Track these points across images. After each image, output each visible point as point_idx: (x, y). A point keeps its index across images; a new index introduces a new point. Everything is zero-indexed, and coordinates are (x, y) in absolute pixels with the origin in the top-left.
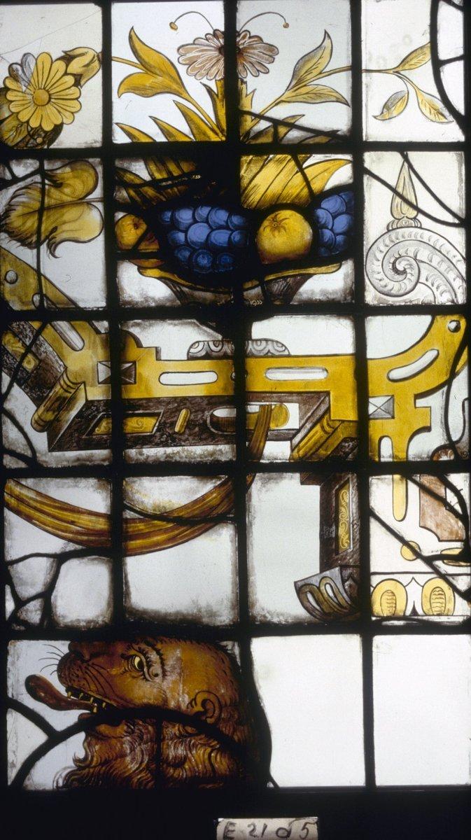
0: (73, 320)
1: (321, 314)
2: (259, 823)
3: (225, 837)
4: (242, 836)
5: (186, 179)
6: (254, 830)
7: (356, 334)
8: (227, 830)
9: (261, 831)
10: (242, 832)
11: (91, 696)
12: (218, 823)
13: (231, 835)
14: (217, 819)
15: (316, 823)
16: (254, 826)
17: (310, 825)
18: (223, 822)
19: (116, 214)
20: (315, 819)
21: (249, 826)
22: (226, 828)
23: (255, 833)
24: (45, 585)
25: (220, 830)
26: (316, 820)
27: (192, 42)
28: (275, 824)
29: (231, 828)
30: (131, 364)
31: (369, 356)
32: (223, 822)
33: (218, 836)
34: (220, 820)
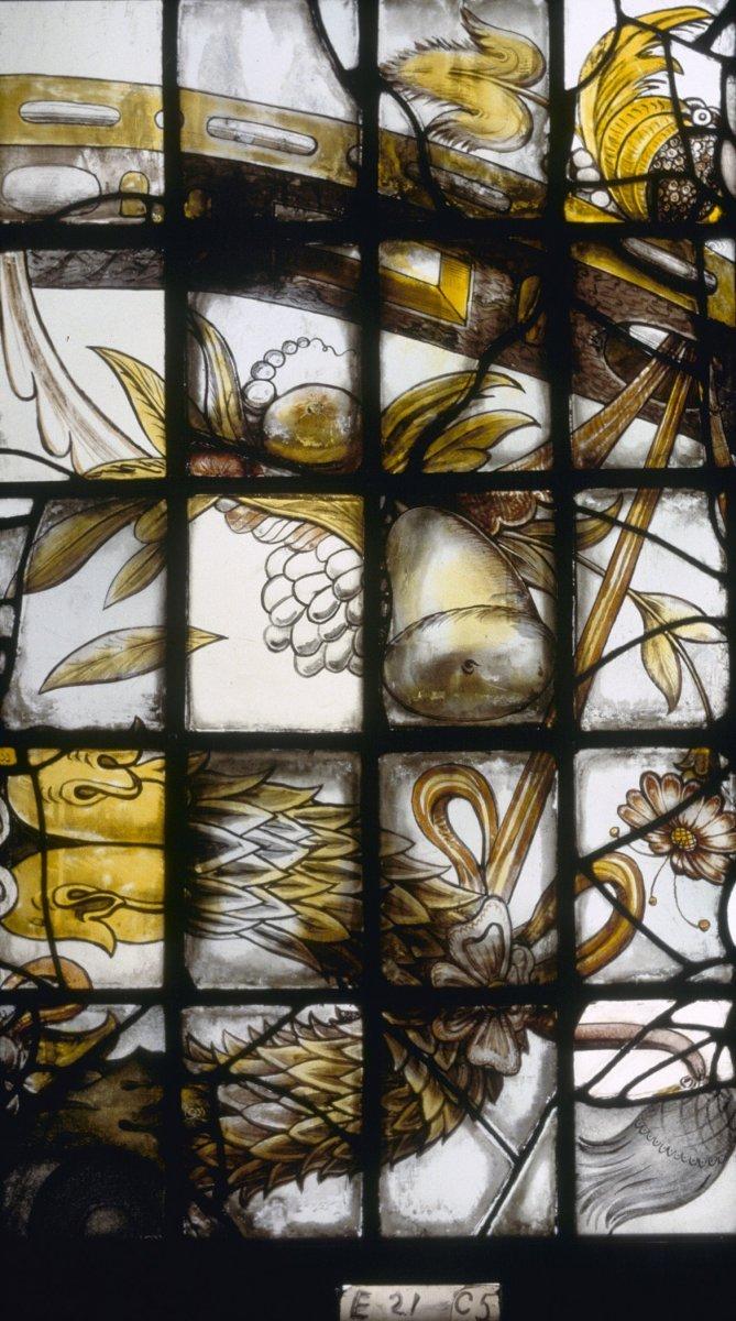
0: (41, 248)
1: (549, 406)
2: (408, 1292)
3: (354, 1315)
4: (380, 1312)
5: (279, 209)
6: (399, 1304)
7: (73, 1064)
8: (356, 1305)
9: (410, 1306)
10: (380, 1306)
11: (629, 383)
12: (341, 1293)
13: (362, 1311)
14: (340, 1286)
15: (498, 1293)
16: (400, 1298)
17: (484, 1296)
18: (350, 1291)
19: (191, 503)
20: (495, 1286)
21: (391, 1297)
22: (355, 1300)
23: (400, 1310)
24: (613, 980)
25: (346, 1303)
26: (497, 1288)
27: (240, 833)
28: (436, 1295)
29: (363, 1301)
30: (263, 1078)
31: (160, 946)
32: (350, 1291)
33: (342, 1313)
34: (345, 1287)
